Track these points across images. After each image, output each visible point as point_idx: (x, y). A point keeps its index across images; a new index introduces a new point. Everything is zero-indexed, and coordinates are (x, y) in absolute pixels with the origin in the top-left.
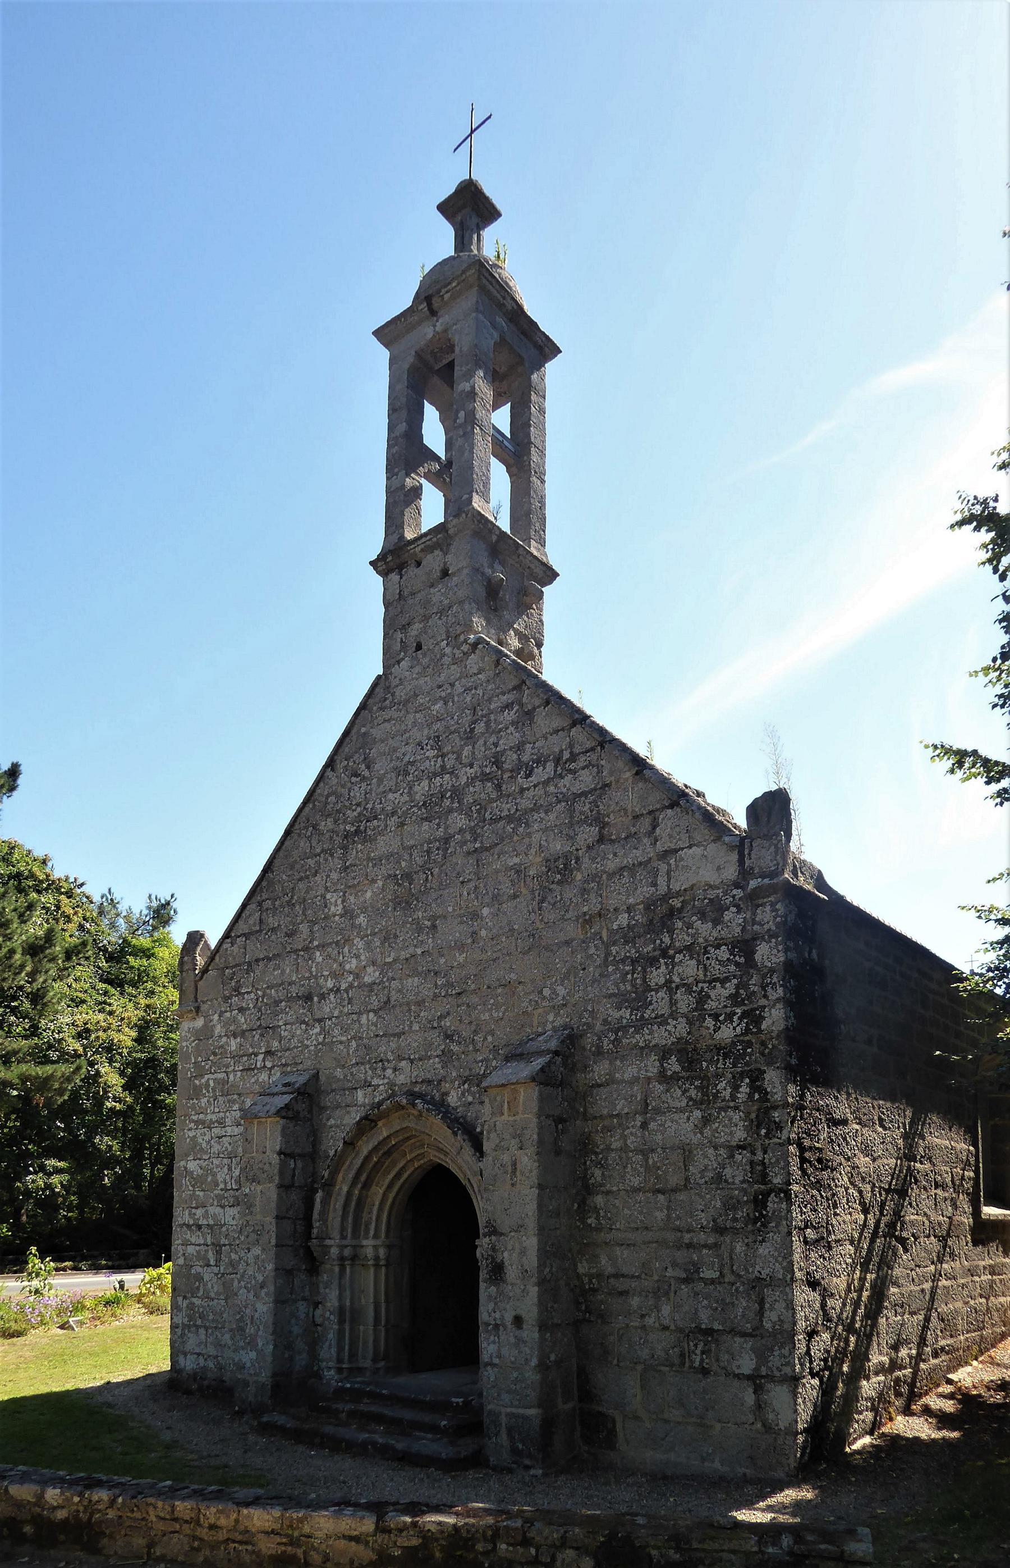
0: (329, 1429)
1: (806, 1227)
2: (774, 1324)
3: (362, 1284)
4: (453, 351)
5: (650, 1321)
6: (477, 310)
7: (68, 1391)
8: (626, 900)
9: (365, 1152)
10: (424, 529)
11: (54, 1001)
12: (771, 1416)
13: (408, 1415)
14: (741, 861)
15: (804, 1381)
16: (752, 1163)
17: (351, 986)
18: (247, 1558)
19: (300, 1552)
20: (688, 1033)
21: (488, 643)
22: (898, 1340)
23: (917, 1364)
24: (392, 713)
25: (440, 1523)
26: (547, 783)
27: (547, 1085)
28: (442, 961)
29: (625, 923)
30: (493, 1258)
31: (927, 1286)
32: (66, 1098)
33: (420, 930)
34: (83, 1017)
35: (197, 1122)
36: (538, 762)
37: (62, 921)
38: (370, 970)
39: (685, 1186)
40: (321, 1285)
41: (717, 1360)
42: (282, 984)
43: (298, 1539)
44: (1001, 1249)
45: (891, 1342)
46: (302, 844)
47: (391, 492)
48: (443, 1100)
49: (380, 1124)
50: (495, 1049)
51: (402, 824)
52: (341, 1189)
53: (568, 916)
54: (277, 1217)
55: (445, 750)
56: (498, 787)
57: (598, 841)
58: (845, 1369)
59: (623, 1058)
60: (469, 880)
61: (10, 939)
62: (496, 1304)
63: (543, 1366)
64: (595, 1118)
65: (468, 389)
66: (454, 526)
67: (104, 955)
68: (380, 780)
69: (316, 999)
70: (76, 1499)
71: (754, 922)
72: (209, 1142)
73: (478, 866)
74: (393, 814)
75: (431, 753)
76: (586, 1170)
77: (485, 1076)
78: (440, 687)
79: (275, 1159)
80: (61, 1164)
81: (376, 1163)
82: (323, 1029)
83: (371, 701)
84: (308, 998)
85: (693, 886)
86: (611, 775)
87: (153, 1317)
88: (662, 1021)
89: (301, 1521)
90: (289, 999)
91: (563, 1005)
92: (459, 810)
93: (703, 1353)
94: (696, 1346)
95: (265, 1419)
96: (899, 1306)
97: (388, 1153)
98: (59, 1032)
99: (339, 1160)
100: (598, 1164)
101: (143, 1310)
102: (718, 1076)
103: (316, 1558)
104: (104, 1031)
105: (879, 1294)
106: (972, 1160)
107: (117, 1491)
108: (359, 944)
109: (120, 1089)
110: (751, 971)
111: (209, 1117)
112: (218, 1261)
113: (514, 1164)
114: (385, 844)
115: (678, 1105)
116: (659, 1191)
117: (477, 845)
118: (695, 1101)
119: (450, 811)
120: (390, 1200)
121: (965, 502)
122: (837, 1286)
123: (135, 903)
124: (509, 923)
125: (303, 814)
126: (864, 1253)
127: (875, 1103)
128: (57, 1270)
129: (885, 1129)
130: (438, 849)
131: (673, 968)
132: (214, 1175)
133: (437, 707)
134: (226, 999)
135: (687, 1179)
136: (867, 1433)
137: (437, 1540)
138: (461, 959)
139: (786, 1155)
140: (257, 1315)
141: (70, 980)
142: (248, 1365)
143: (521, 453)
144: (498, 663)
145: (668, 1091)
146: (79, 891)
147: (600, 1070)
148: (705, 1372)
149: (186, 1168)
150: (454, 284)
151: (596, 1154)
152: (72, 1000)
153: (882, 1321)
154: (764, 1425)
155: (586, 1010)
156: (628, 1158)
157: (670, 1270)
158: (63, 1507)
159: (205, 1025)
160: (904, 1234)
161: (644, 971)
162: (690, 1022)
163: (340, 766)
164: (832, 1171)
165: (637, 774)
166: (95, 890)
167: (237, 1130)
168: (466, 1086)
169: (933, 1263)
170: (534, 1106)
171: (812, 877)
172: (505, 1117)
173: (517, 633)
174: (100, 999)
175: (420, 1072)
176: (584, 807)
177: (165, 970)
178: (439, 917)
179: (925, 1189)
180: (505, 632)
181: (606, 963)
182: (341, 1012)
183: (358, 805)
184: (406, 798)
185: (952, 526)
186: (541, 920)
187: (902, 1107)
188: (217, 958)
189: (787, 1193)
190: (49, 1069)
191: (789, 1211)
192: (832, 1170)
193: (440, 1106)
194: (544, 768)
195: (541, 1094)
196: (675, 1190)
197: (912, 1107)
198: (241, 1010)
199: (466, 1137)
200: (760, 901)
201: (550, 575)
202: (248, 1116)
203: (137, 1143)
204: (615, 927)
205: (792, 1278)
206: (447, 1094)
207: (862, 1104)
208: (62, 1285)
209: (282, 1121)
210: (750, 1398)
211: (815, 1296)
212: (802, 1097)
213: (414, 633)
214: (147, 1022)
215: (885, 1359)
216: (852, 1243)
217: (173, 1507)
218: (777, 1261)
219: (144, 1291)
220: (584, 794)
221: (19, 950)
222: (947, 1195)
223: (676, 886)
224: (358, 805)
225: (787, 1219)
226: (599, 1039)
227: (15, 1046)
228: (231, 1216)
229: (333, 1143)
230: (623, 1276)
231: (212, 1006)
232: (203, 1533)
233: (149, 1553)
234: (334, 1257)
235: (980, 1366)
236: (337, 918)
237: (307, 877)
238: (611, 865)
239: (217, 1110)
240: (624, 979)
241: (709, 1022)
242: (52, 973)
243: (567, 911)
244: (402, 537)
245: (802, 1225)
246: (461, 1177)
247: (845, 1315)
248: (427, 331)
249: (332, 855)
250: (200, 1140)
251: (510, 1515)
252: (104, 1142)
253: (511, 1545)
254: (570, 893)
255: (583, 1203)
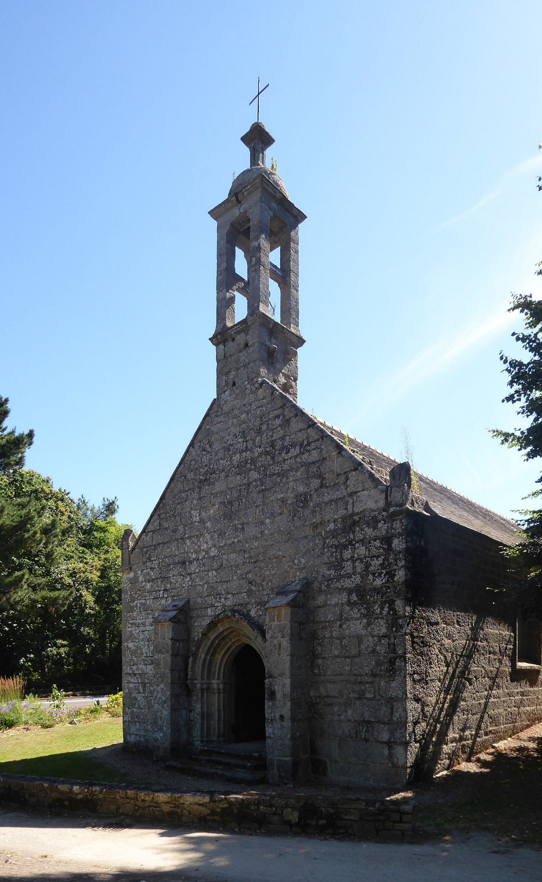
0: (197, 768)
1: (414, 673)
2: (398, 718)
3: (212, 701)
4: (250, 222)
5: (342, 717)
6: (261, 201)
7: (76, 752)
8: (333, 516)
9: (212, 638)
10: (237, 320)
11: (57, 557)
12: (395, 760)
13: (233, 761)
14: (386, 498)
15: (411, 744)
16: (389, 644)
17: (204, 557)
18: (158, 813)
19: (179, 810)
20: (361, 582)
21: (268, 383)
22: (464, 727)
23: (475, 738)
24: (221, 419)
25: (236, 798)
26: (296, 457)
27: (295, 607)
28: (247, 545)
29: (333, 528)
30: (271, 689)
31: (483, 701)
32: (66, 608)
33: (236, 530)
34: (73, 565)
35: (132, 624)
36: (292, 445)
37: (59, 515)
38: (213, 549)
39: (359, 654)
40: (193, 702)
41: (372, 735)
42: (171, 556)
43: (178, 805)
44: (528, 683)
45: (460, 727)
46: (179, 486)
47: (220, 300)
48: (248, 614)
49: (219, 625)
50: (272, 589)
51: (227, 476)
52: (201, 656)
53: (306, 524)
54: (171, 670)
55: (247, 439)
56: (273, 458)
57: (320, 487)
58: (434, 739)
59: (331, 594)
60: (260, 505)
61: (34, 526)
62: (272, 710)
63: (293, 738)
64: (318, 622)
65: (257, 245)
66: (250, 321)
67: (81, 531)
68: (216, 454)
69: (187, 563)
70: (86, 790)
71: (392, 529)
72: (138, 634)
73: (264, 498)
74: (223, 471)
75: (241, 440)
76: (314, 647)
77: (267, 602)
78: (244, 405)
79: (169, 642)
80: (65, 642)
81: (217, 644)
82: (191, 578)
83: (211, 412)
84: (184, 563)
85: (364, 510)
86: (327, 454)
87: (114, 718)
88: (349, 576)
89: (179, 797)
90: (174, 564)
91: (304, 568)
92: (255, 470)
93: (366, 732)
94: (363, 728)
95: (168, 763)
96: (466, 711)
97: (223, 639)
98: (61, 574)
99: (200, 641)
100: (319, 644)
101: (109, 715)
102: (374, 603)
103: (186, 813)
104: (84, 573)
105: (454, 706)
106: (512, 640)
107: (103, 787)
108: (208, 536)
109: (93, 603)
110: (390, 552)
111: (138, 621)
112: (144, 691)
113: (280, 645)
114: (219, 486)
115: (356, 616)
116: (347, 657)
117: (263, 488)
118: (364, 615)
119: (250, 470)
120: (224, 662)
121: (515, 298)
122: (430, 701)
123: (96, 503)
124: (279, 527)
125: (179, 470)
126: (446, 686)
127: (455, 614)
128: (65, 696)
129: (460, 626)
130: (244, 489)
131: (355, 550)
132: (141, 649)
133: (243, 416)
134: (144, 563)
135: (360, 652)
136: (446, 770)
137: (235, 805)
138: (256, 544)
139: (405, 640)
140: (163, 716)
141: (65, 546)
142: (160, 739)
143: (285, 276)
144: (272, 394)
145: (351, 609)
146: (67, 497)
147: (321, 600)
148: (366, 740)
149: (127, 646)
150: (249, 187)
151: (319, 640)
152: (66, 557)
153: (456, 718)
154: (392, 764)
155: (314, 570)
156: (333, 642)
157: (352, 694)
158: (81, 794)
159: (134, 576)
160: (470, 677)
161: (341, 552)
162: (362, 577)
163: (197, 446)
164: (429, 647)
165: (339, 453)
166: (75, 496)
167: (151, 628)
168: (259, 607)
169: (486, 690)
170: (289, 617)
171: (422, 505)
172: (276, 623)
173: (284, 374)
174: (81, 555)
175: (237, 600)
176: (313, 469)
177: (113, 539)
178: (246, 523)
179: (483, 654)
180: (277, 375)
181: (323, 548)
182: (199, 570)
183: (206, 466)
184: (229, 463)
185: (509, 310)
186: (294, 526)
187: (471, 615)
188: (139, 542)
189: (405, 658)
190: (56, 593)
191: (405, 666)
192: (430, 646)
193: (247, 617)
194: (295, 449)
195: (292, 611)
196: (354, 657)
197: (476, 614)
198: (152, 569)
199: (258, 631)
200: (395, 518)
201: (301, 342)
202: (156, 621)
203: (101, 631)
204: (328, 530)
205: (406, 698)
206: (250, 610)
207: (447, 614)
208: (70, 703)
209: (172, 624)
210: (386, 752)
211: (418, 706)
212: (414, 612)
213: (232, 377)
214: (105, 567)
215: (457, 736)
216: (439, 681)
217: (126, 793)
218: (399, 689)
219: (109, 706)
220: (314, 463)
221: (39, 532)
222: (496, 657)
223: (356, 510)
224: (206, 466)
225: (404, 670)
226: (320, 584)
227: (39, 581)
228: (149, 669)
229: (197, 634)
230: (330, 697)
231: (138, 567)
232: (139, 803)
233: (117, 812)
234: (198, 688)
235: (512, 740)
236: (197, 523)
237: (182, 502)
238: (326, 499)
239: (141, 618)
240: (332, 556)
241: (371, 577)
242: (56, 543)
243: (306, 521)
244: (225, 325)
245: (412, 673)
246: (257, 650)
247: (434, 714)
248: (236, 212)
249: (194, 491)
250: (134, 633)
251: (265, 795)
252: (86, 630)
253: (265, 806)
254: (307, 512)
255: (312, 663)
